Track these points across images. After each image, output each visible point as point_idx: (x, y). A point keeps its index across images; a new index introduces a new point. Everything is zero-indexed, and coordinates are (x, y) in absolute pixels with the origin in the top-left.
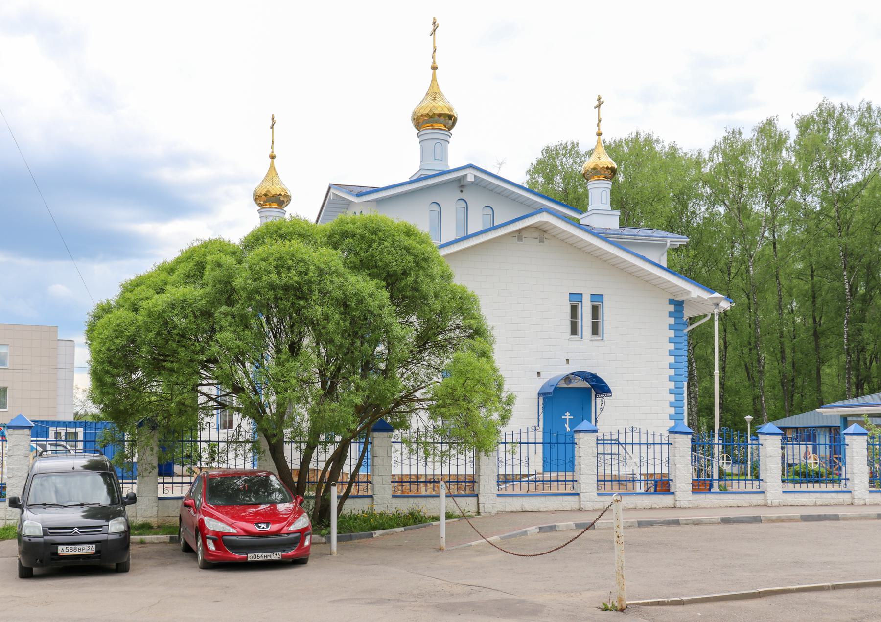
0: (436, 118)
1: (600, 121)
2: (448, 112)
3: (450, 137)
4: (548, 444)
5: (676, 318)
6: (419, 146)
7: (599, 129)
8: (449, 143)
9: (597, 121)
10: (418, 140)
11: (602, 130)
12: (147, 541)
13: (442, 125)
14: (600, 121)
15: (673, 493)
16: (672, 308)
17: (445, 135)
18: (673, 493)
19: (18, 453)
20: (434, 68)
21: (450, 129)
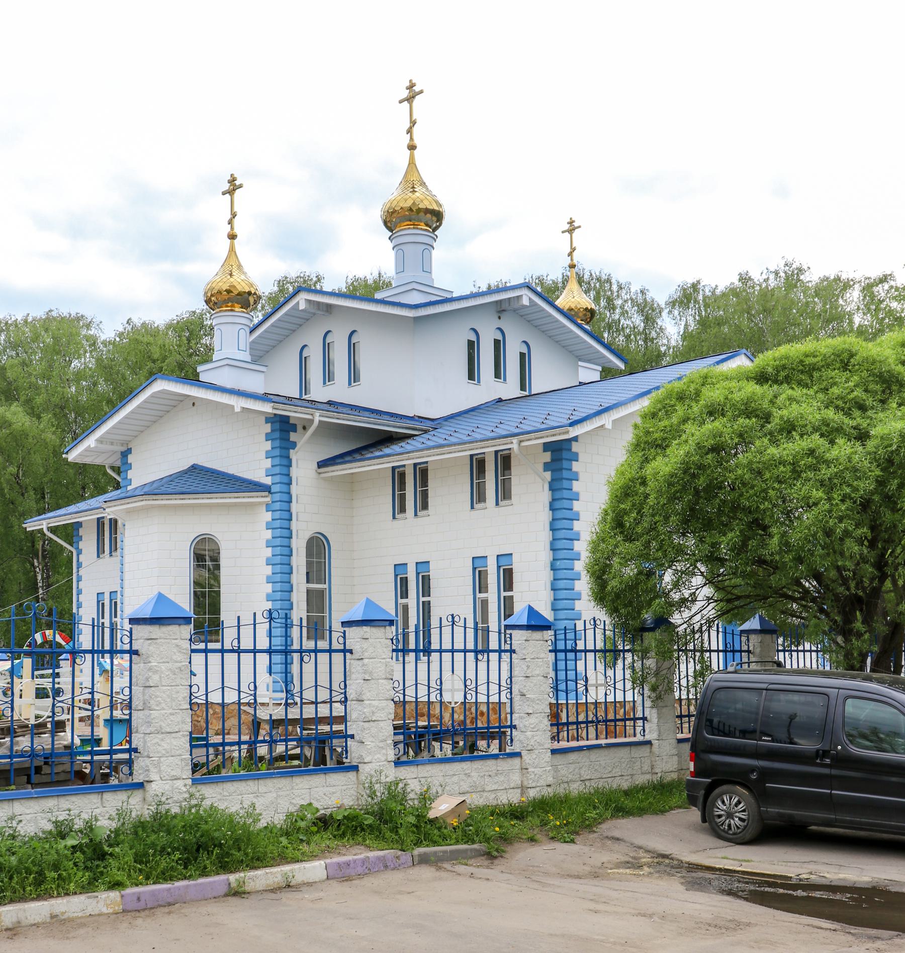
0: (422, 214)
1: (234, 215)
2: (436, 208)
3: (435, 241)
4: (312, 703)
5: (553, 471)
6: (392, 254)
7: (232, 228)
8: (433, 248)
9: (229, 216)
10: (390, 245)
11: (237, 230)
12: (299, 878)
13: (422, 224)
14: (234, 215)
15: (355, 768)
16: (547, 457)
17: (428, 238)
18: (355, 768)
19: (537, 672)
20: (412, 147)
21: (434, 230)
